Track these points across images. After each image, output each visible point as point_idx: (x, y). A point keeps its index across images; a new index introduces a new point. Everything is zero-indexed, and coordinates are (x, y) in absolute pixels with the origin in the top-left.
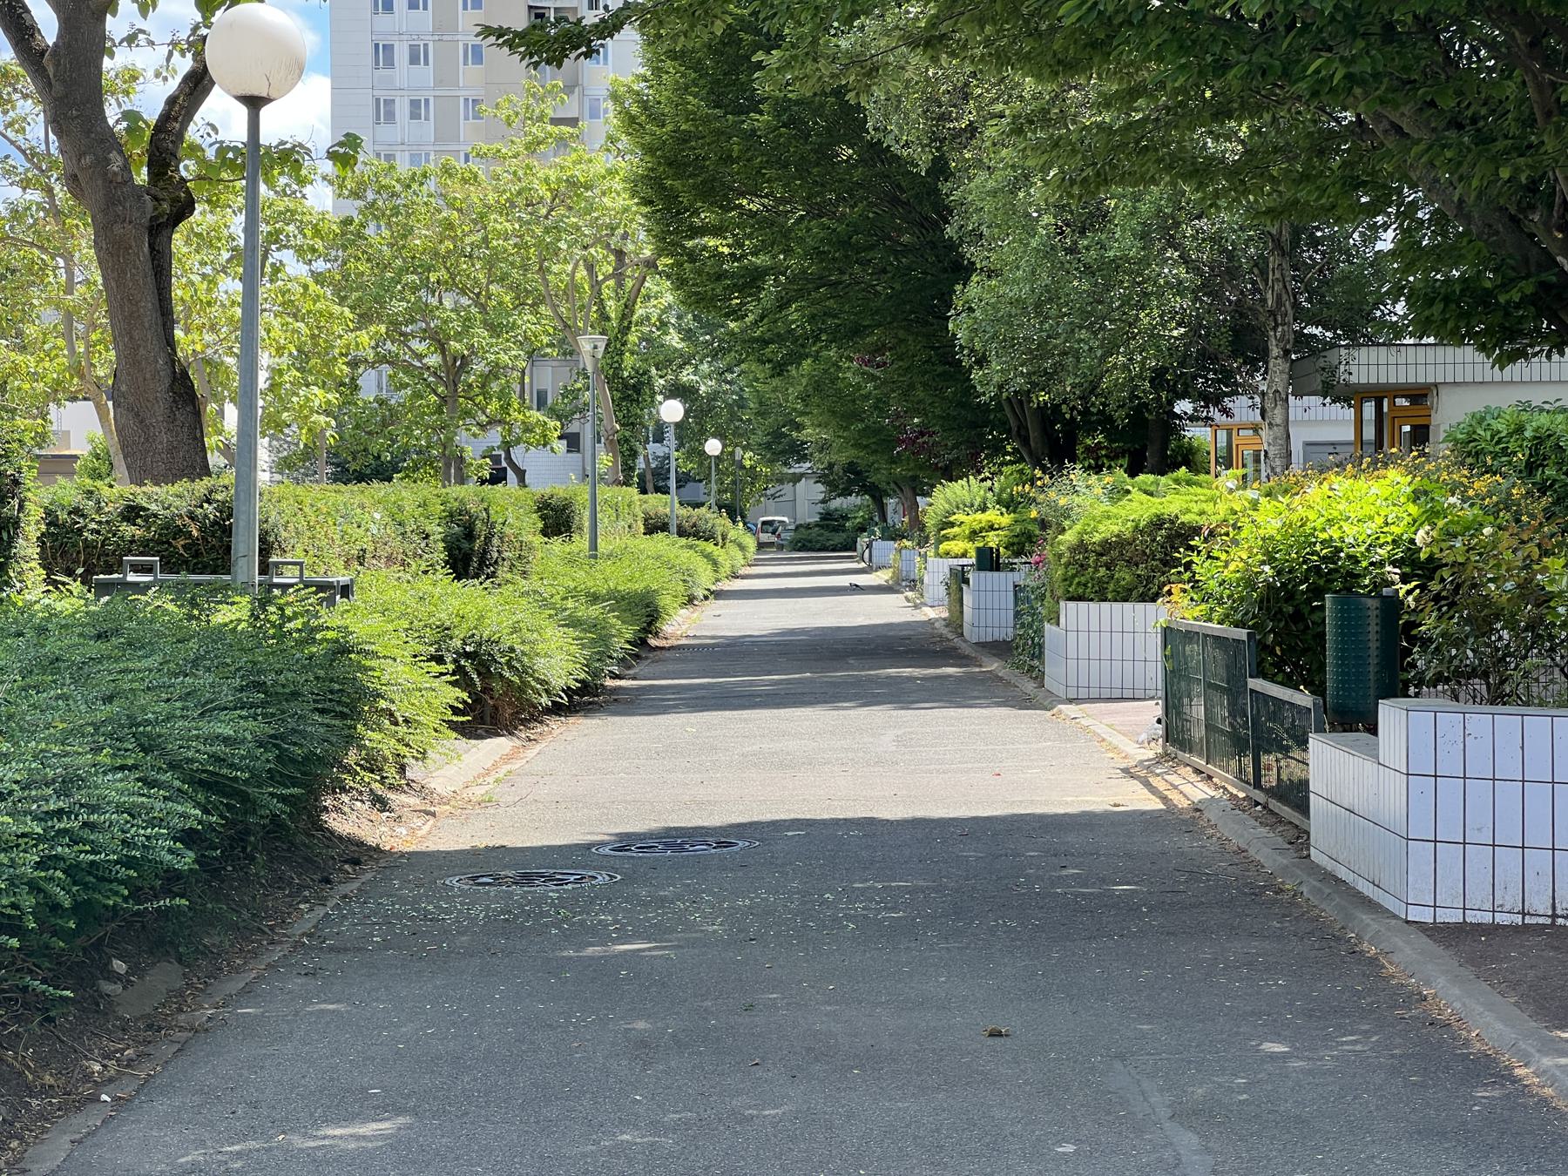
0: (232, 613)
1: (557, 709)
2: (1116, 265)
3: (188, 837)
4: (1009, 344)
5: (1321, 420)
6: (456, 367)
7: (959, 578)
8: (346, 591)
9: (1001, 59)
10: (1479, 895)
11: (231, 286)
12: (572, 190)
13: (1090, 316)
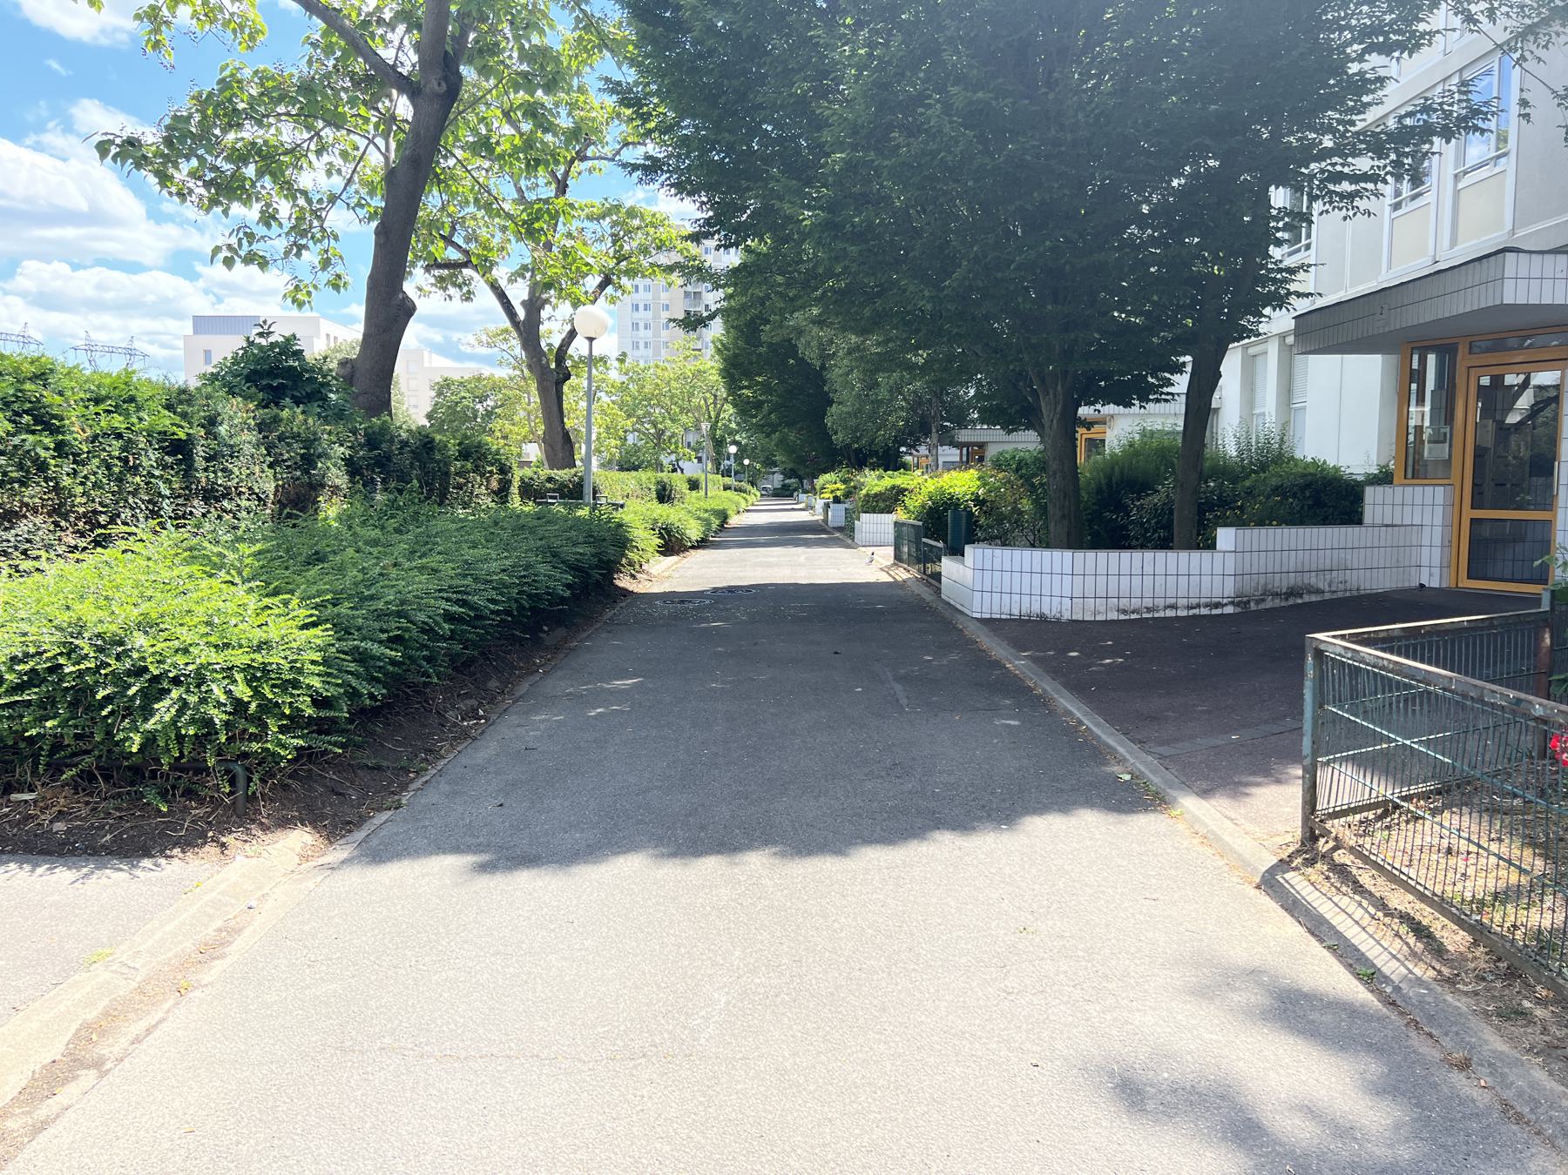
0: (583, 513)
1: (693, 547)
2: (881, 401)
3: (568, 586)
4: (845, 428)
5: (949, 454)
6: (660, 433)
7: (827, 506)
8: (622, 506)
9: (844, 329)
10: (996, 609)
11: (583, 404)
12: (699, 373)
13: (873, 416)
